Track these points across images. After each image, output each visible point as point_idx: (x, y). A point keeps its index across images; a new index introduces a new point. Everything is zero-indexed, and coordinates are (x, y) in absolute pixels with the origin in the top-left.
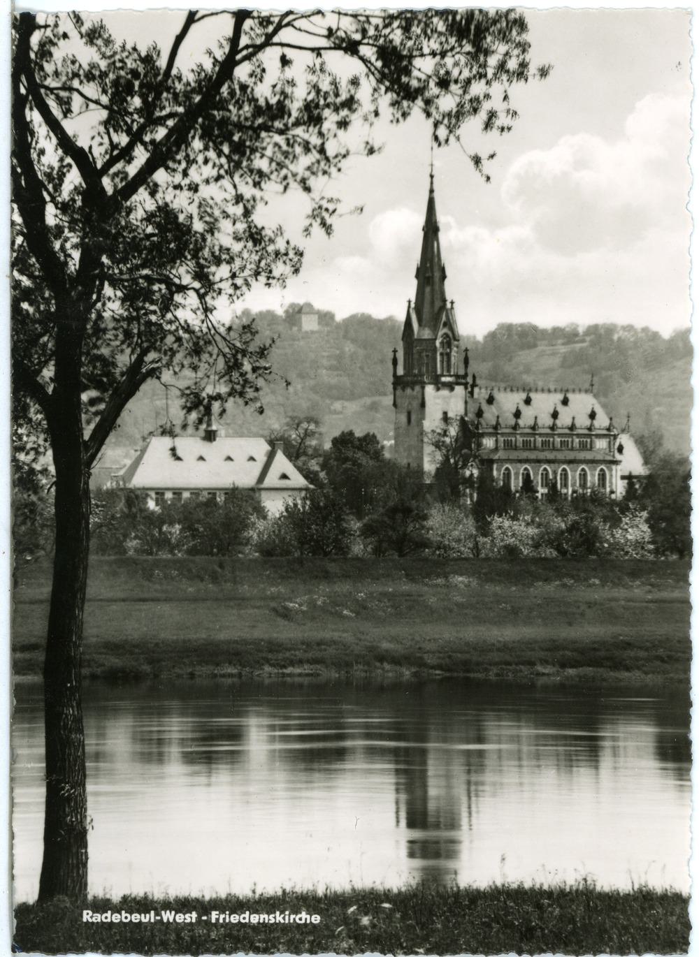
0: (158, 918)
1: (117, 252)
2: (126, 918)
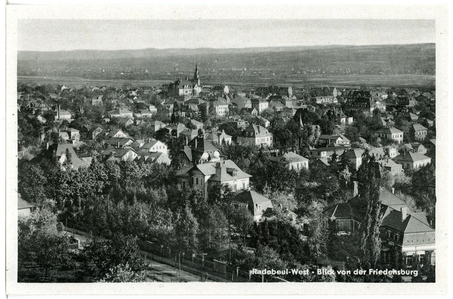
0: (290, 272)
1: (417, 108)
2: (274, 272)
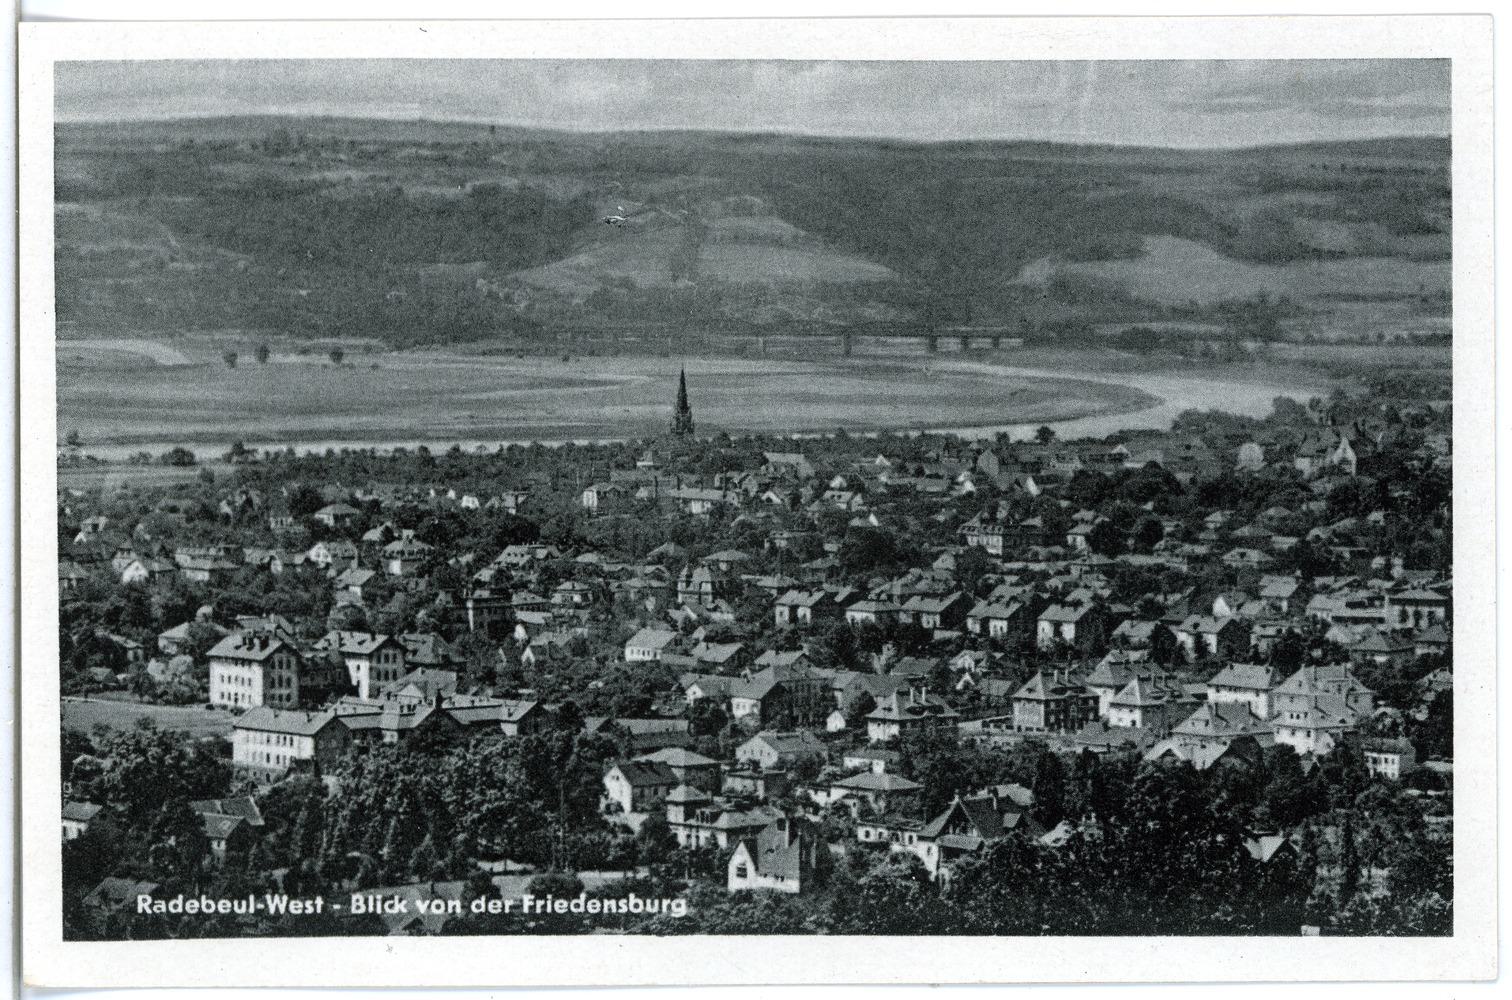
2: (636, 906)
